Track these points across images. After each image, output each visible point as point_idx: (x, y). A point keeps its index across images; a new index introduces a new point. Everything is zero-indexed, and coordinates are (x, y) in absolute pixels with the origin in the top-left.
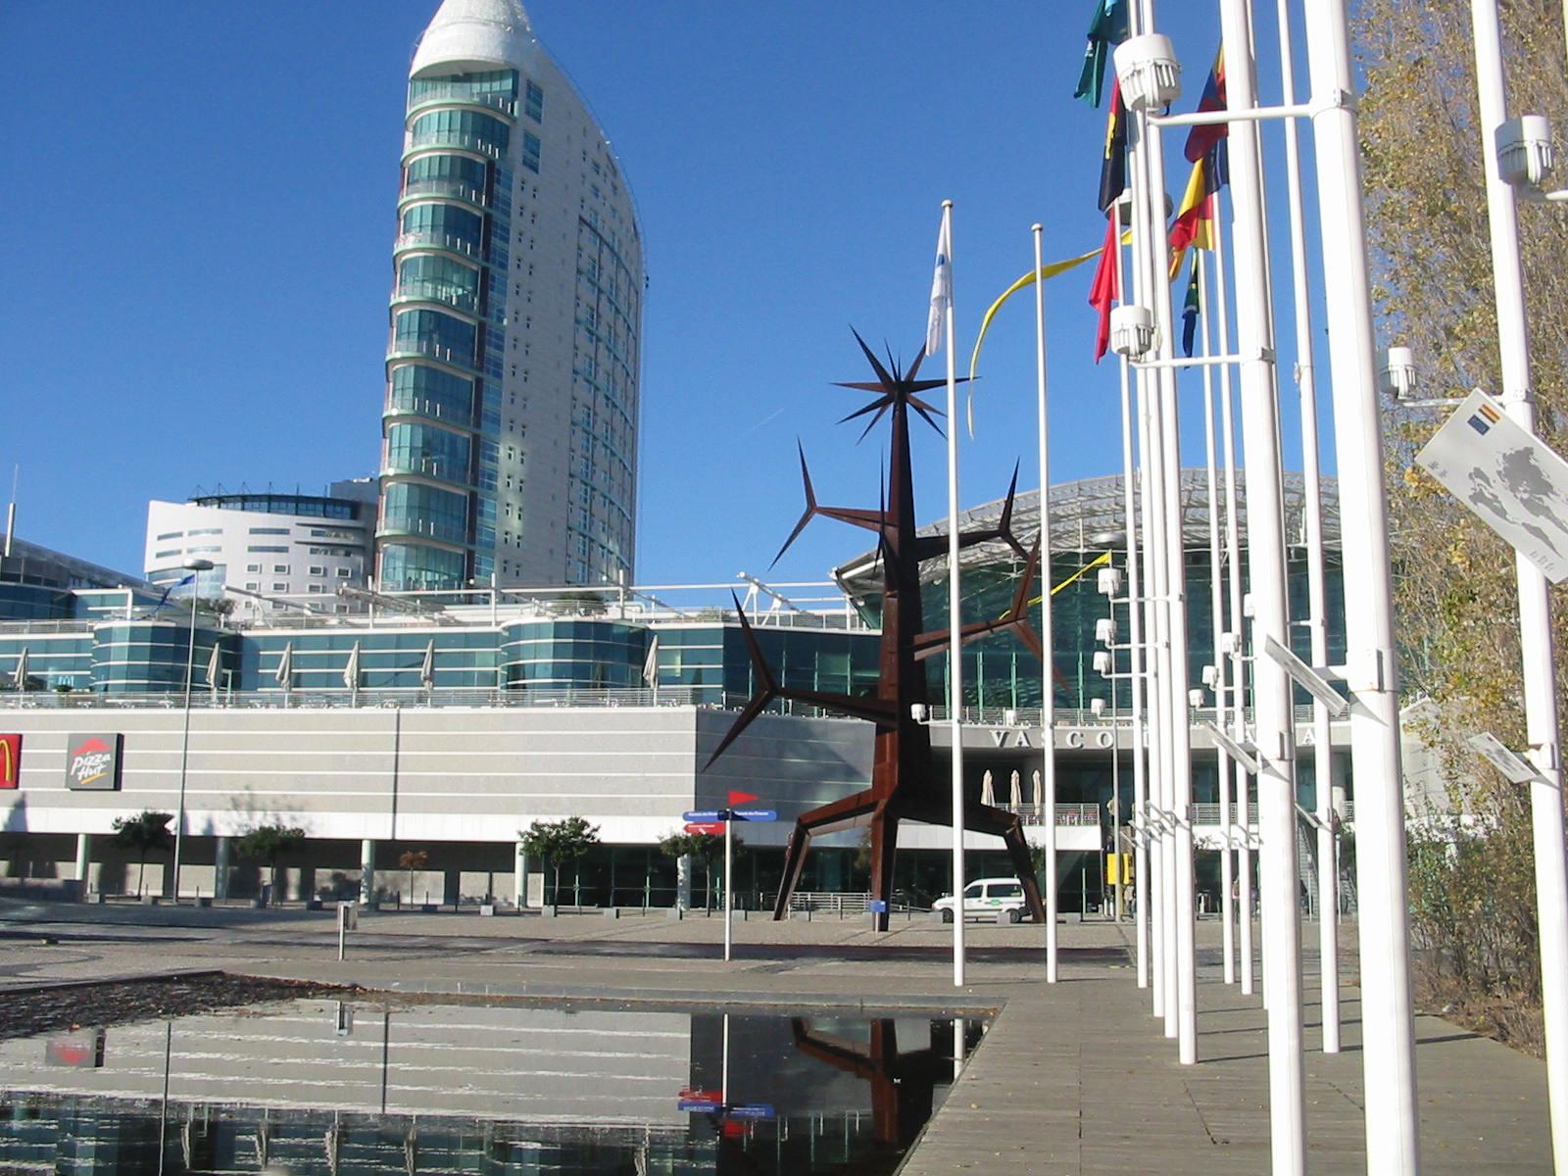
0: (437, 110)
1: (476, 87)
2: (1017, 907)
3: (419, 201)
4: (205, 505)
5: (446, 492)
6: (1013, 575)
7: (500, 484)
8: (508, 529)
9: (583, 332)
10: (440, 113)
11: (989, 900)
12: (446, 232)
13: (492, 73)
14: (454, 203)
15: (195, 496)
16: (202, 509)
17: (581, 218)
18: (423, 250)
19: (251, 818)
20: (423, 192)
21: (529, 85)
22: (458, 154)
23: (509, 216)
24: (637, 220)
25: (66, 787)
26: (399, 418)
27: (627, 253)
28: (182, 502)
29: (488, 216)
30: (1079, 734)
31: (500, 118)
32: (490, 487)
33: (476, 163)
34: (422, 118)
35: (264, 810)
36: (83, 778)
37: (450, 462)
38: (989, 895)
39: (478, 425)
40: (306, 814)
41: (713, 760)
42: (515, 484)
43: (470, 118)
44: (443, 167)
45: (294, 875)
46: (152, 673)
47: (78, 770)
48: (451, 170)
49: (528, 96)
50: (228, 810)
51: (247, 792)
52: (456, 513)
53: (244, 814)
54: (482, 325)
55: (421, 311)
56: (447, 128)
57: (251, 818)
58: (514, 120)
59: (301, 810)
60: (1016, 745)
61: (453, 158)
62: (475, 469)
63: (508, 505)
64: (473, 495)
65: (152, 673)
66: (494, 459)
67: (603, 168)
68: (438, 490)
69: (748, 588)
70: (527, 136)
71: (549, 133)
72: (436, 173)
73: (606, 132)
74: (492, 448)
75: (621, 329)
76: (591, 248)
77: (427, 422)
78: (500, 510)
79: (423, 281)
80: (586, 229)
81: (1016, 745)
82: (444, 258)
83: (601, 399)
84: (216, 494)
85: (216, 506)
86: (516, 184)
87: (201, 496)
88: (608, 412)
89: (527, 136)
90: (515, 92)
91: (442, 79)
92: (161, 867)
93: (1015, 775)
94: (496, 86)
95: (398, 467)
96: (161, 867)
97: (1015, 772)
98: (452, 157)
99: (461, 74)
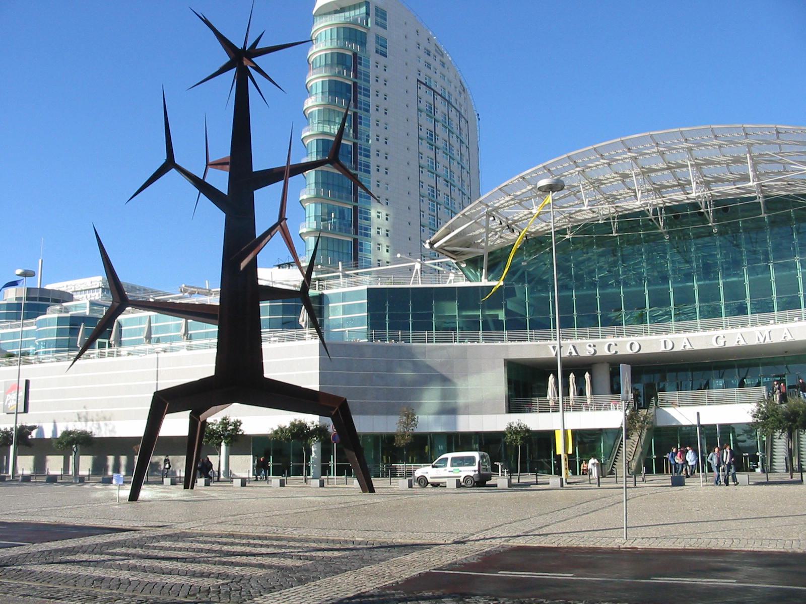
0: (324, 30)
1: (347, 14)
2: (472, 474)
3: (316, 79)
4: (283, 268)
5: (339, 240)
6: (567, 237)
7: (373, 232)
8: (379, 259)
9: (424, 143)
10: (331, 29)
11: (452, 469)
12: (329, 95)
13: (355, 5)
14: (334, 78)
15: (277, 264)
16: (281, 270)
17: (418, 80)
18: (317, 106)
19: (86, 426)
20: (318, 74)
21: (377, 9)
22: (335, 51)
23: (369, 83)
24: (463, 81)
25: (4, 412)
26: (309, 200)
27: (456, 100)
28: (272, 268)
29: (355, 84)
30: (613, 344)
31: (360, 29)
32: (367, 235)
33: (346, 55)
34: (321, 33)
35: (93, 421)
36: (11, 407)
37: (340, 224)
38: (452, 466)
39: (356, 201)
40: (112, 422)
41: (73, 364)
42: (383, 232)
43: (342, 30)
44: (327, 60)
45: (123, 459)
46: (58, 344)
47: (8, 402)
48: (331, 61)
49: (377, 15)
50: (76, 421)
51: (85, 410)
52: (345, 251)
53: (84, 423)
54: (355, 144)
55: (317, 140)
56: (330, 38)
57: (86, 426)
58: (369, 29)
59: (110, 420)
60: (568, 354)
61: (332, 54)
62: (356, 226)
63: (379, 245)
64: (355, 240)
65: (58, 344)
66: (368, 219)
67: (433, 52)
68: (333, 239)
69: (414, 266)
70: (377, 37)
71: (393, 34)
72: (324, 64)
73: (433, 32)
74: (366, 213)
75: (454, 141)
76: (427, 97)
77: (324, 201)
78: (373, 245)
79: (318, 123)
80: (423, 86)
81: (568, 354)
82: (329, 109)
83: (441, 181)
84: (287, 262)
85: (287, 268)
86: (372, 63)
87: (280, 263)
88: (447, 191)
89: (377, 37)
90: (368, 14)
91: (329, 13)
92: (62, 457)
93: (587, 375)
94: (357, 12)
95: (309, 228)
96: (62, 457)
97: (572, 374)
98: (332, 53)
99: (339, 9)
